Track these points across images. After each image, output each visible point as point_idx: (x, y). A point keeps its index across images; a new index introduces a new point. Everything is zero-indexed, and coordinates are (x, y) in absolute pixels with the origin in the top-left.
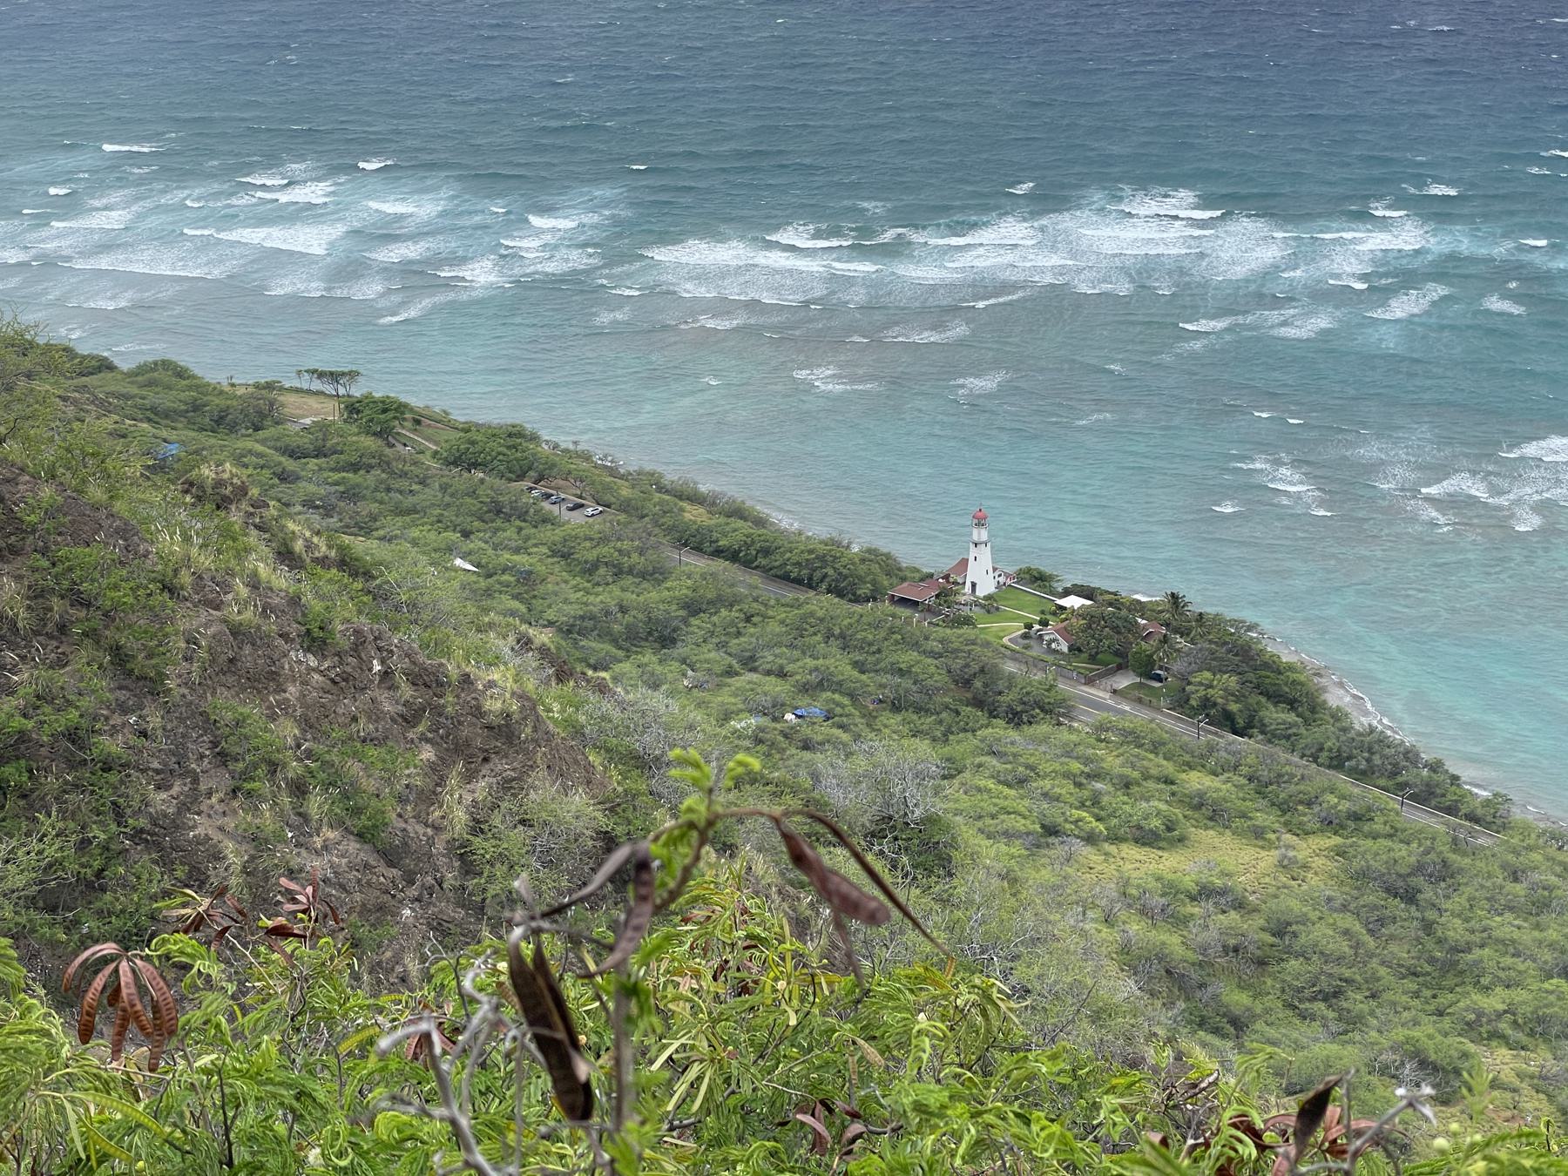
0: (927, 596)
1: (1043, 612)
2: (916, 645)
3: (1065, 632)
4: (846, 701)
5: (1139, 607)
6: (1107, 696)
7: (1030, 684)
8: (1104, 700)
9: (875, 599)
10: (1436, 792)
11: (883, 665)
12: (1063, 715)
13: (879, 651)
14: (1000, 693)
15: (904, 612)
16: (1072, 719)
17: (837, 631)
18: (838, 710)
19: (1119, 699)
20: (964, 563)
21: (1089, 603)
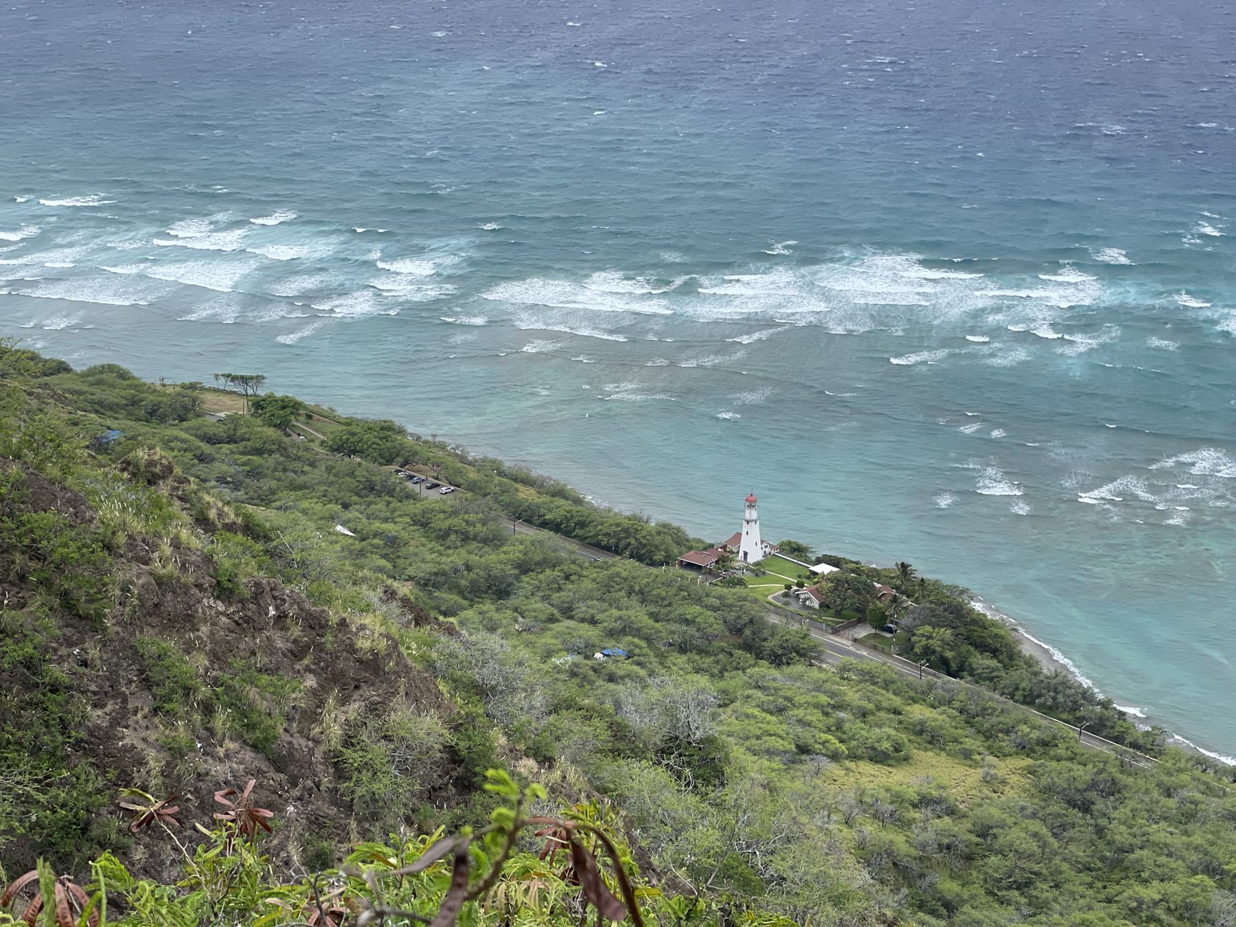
0: (708, 561)
1: (799, 576)
2: (699, 601)
3: (817, 593)
4: (643, 644)
5: (875, 574)
6: (849, 643)
7: (788, 633)
8: (847, 647)
9: (668, 564)
10: (1106, 725)
11: (673, 615)
12: (815, 658)
13: (670, 604)
14: (765, 640)
15: (690, 574)
16: (822, 661)
17: (637, 588)
18: (637, 651)
19: (857, 645)
20: (738, 537)
21: (835, 569)
